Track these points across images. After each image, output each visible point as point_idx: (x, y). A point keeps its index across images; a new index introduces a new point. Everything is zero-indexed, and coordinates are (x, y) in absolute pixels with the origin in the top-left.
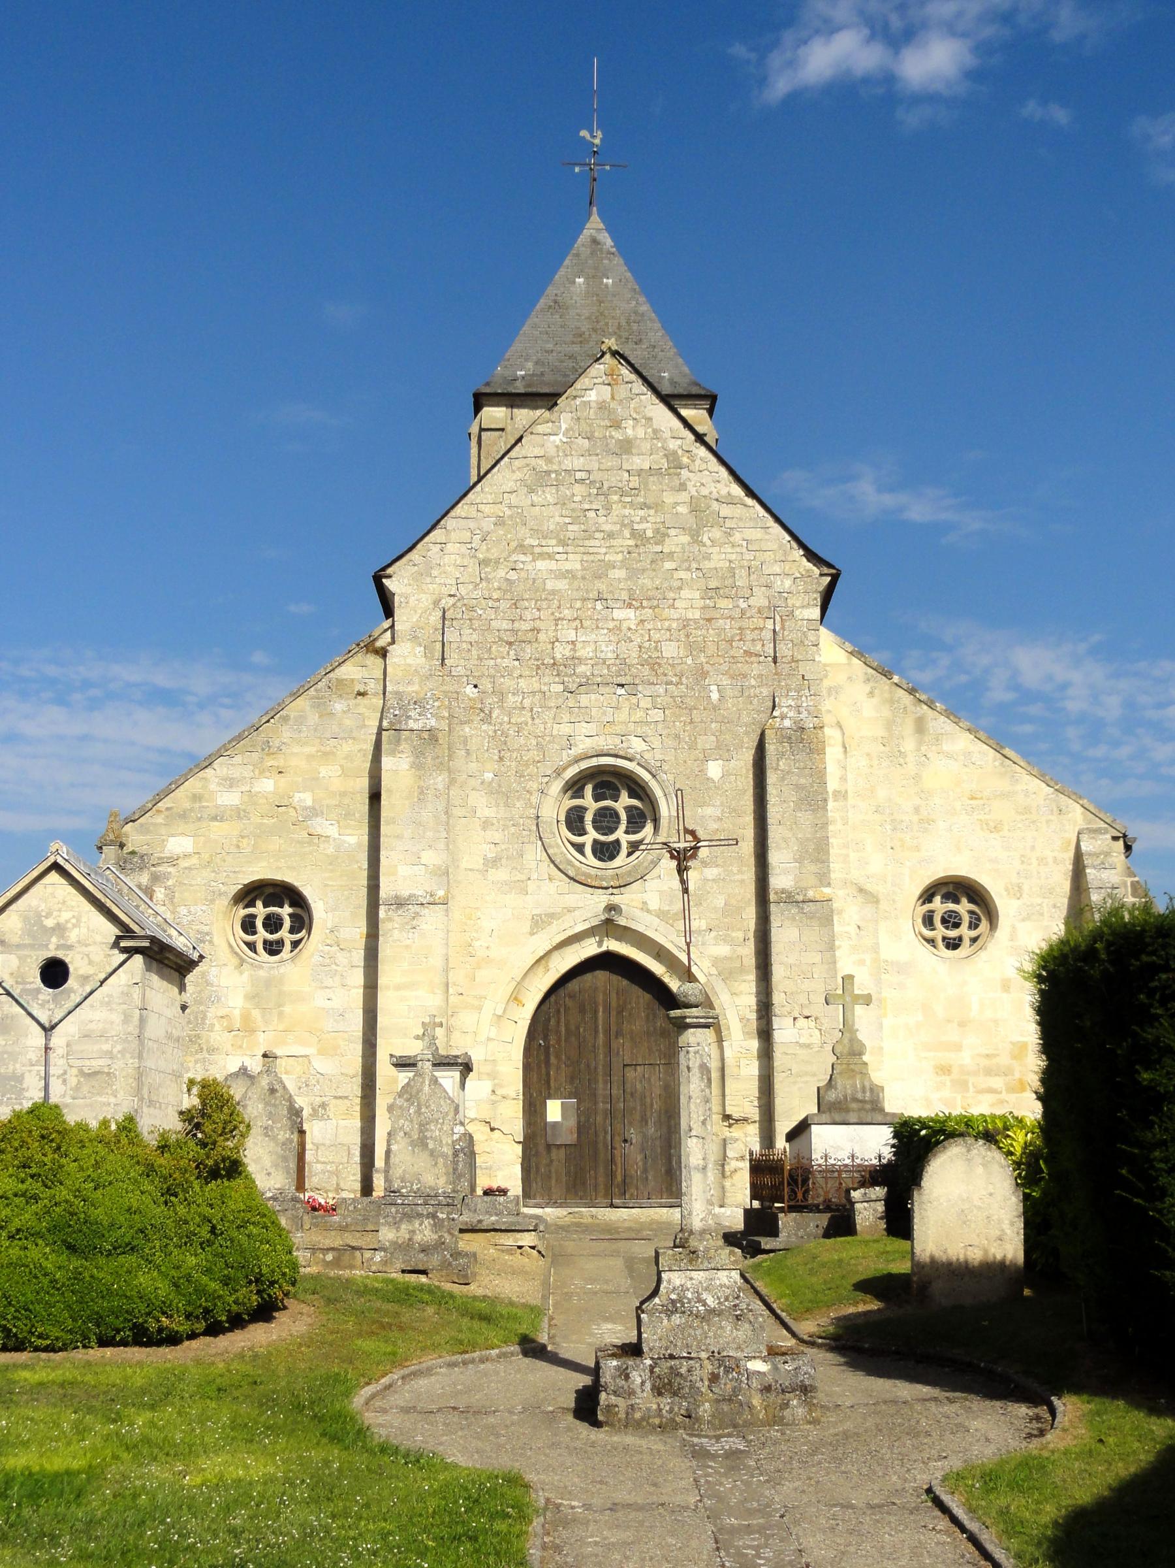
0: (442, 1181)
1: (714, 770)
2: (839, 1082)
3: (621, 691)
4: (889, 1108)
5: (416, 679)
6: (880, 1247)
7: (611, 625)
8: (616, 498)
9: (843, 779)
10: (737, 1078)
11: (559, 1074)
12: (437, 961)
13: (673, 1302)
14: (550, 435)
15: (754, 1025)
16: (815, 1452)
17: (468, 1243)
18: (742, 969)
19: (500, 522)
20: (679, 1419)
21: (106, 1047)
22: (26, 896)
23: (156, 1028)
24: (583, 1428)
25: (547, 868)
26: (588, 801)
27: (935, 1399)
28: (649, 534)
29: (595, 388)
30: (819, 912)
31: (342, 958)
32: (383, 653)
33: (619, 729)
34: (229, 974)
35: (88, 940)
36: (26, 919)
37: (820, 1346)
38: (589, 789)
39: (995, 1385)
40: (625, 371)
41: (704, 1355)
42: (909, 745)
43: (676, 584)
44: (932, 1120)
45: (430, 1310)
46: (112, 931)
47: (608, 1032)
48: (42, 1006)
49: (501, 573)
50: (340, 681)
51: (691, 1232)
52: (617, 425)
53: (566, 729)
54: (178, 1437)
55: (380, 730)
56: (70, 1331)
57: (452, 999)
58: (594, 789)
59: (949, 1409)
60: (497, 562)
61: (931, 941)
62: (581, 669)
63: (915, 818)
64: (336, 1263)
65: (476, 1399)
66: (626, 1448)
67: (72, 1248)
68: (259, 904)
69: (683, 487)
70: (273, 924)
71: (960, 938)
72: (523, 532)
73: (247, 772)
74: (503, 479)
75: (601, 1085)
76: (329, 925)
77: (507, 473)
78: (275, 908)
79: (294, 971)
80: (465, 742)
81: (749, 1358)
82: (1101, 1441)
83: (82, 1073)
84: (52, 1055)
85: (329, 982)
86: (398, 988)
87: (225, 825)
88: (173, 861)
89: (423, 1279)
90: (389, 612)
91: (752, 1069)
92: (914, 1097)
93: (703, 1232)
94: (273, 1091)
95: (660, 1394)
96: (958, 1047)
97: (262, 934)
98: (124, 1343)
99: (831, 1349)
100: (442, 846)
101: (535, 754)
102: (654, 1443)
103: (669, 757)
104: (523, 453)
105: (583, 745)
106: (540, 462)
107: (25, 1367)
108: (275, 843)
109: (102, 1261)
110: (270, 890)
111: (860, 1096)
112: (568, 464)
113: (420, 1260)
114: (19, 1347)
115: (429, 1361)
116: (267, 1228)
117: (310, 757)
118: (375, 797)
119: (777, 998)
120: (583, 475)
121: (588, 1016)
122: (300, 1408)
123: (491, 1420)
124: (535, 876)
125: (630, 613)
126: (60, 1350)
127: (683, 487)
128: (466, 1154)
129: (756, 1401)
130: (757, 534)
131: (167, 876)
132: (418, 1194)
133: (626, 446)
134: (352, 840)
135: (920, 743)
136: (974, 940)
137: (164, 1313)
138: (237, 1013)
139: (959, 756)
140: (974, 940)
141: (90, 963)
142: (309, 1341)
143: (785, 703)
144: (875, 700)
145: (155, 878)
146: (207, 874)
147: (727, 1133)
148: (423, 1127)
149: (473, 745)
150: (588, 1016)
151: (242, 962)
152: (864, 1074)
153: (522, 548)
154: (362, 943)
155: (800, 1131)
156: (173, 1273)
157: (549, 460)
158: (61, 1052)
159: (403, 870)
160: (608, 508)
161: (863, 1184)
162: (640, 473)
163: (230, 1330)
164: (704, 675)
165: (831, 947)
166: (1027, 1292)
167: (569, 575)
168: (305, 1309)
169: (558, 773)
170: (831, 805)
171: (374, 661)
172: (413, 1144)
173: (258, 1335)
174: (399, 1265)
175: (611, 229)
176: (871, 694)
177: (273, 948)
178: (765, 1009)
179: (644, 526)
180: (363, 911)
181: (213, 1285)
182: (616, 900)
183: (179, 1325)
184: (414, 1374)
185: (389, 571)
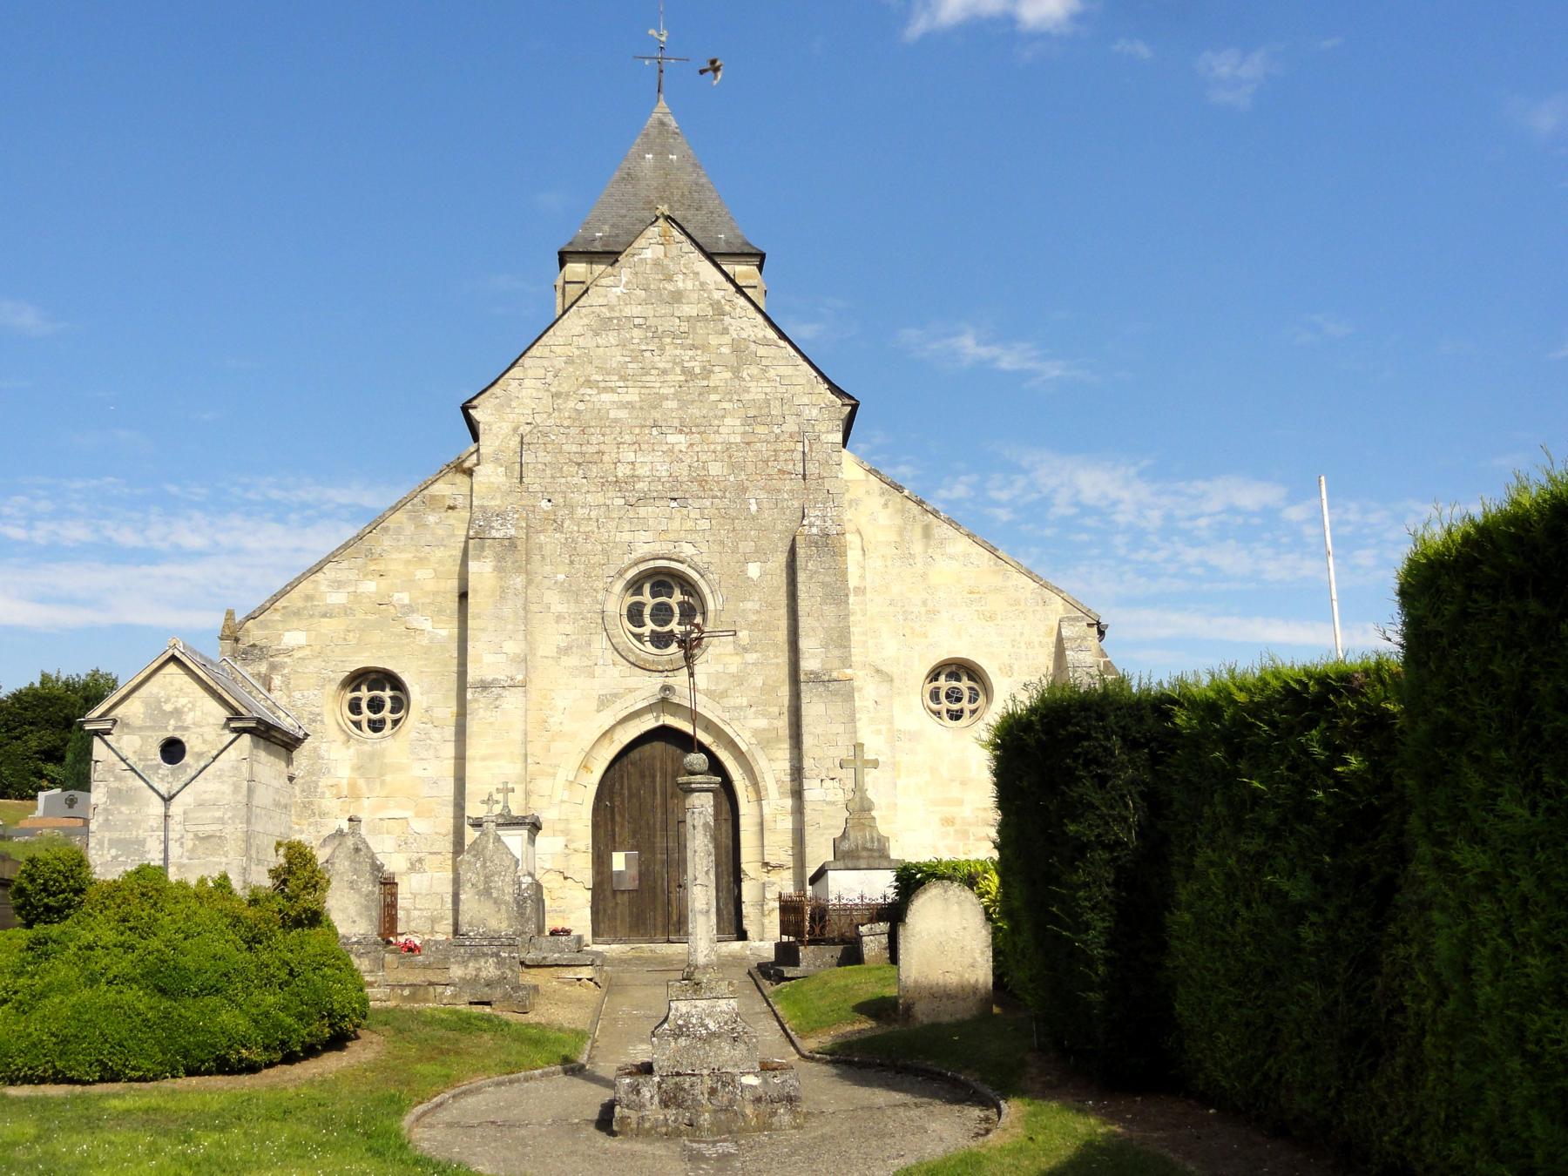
0: (504, 925)
1: (753, 570)
2: (852, 834)
3: (673, 504)
4: (895, 854)
5: (498, 495)
6: (880, 973)
7: (665, 448)
8: (668, 340)
9: (862, 577)
10: (774, 831)
11: (623, 831)
12: (518, 737)
13: (680, 1027)
14: (612, 288)
15: (788, 786)
16: (793, 1153)
17: (529, 978)
18: (778, 739)
19: (570, 360)
20: (683, 1127)
21: (218, 814)
22: (148, 685)
23: (263, 797)
24: (602, 1139)
25: (611, 655)
26: (647, 598)
27: (905, 1105)
28: (697, 370)
29: (650, 248)
30: (841, 690)
31: (435, 734)
32: (469, 473)
33: (672, 536)
34: (335, 748)
35: (202, 722)
36: (147, 704)
37: (818, 1061)
38: (647, 588)
39: (959, 1094)
40: (676, 233)
41: (705, 1072)
42: (918, 548)
43: (720, 413)
44: (926, 865)
45: (487, 1037)
46: (224, 713)
47: (664, 793)
48: (162, 779)
49: (571, 404)
50: (433, 497)
51: (696, 967)
52: (669, 279)
53: (627, 537)
54: (237, 1154)
55: (468, 538)
56: (161, 1064)
57: (530, 768)
58: (652, 587)
59: (914, 1113)
60: (568, 395)
61: (938, 713)
62: (639, 486)
63: (923, 610)
64: (412, 997)
65: (514, 1113)
66: (633, 1155)
67: (163, 991)
68: (364, 688)
69: (725, 331)
70: (376, 705)
71: (962, 711)
72: (589, 369)
73: (352, 575)
74: (572, 324)
75: (658, 839)
76: (425, 705)
77: (575, 319)
78: (376, 692)
79: (393, 745)
80: (541, 548)
81: (743, 1074)
82: (1031, 1139)
83: (196, 836)
84: (171, 822)
85: (424, 754)
86: (484, 759)
87: (334, 621)
88: (288, 652)
89: (488, 1009)
90: (476, 438)
91: (787, 823)
92: (914, 843)
93: (706, 966)
94: (357, 850)
95: (667, 1106)
96: (960, 803)
97: (367, 714)
98: (209, 1073)
99: (834, 1063)
100: (520, 636)
101: (600, 558)
102: (659, 1149)
103: (715, 560)
104: (589, 302)
105: (642, 550)
106: (604, 310)
107: (117, 1096)
108: (377, 636)
109: (189, 1001)
110: (374, 676)
111: (869, 845)
112: (627, 311)
113: (485, 993)
114: (115, 1078)
115: (480, 1081)
116: (340, 969)
117: (408, 562)
118: (463, 596)
119: (807, 763)
120: (640, 321)
121: (647, 781)
122: (352, 1126)
123: (523, 1132)
124: (601, 662)
125: (681, 438)
126: (152, 1080)
127: (725, 331)
128: (533, 900)
129: (749, 1111)
130: (789, 371)
131: (283, 666)
132: (483, 936)
133: (677, 297)
134: (444, 633)
135: (927, 546)
136: (973, 712)
137: (244, 1046)
138: (345, 782)
139: (958, 560)
140: (973, 712)
141: (204, 741)
142: (374, 1067)
143: (813, 513)
144: (889, 510)
145: (273, 667)
146: (318, 663)
147: (765, 878)
148: (488, 879)
149: (547, 551)
150: (647, 781)
151: (349, 738)
152: (873, 827)
153: (588, 382)
154: (452, 721)
155: (821, 874)
156: (253, 1010)
157: (612, 309)
158: (178, 819)
159: (488, 658)
160: (662, 349)
161: (871, 920)
162: (689, 319)
163: (306, 1058)
164: (745, 490)
165: (853, 719)
166: (996, 1010)
167: (629, 405)
168: (375, 1038)
169: (621, 574)
170: (852, 599)
171: (461, 479)
172: (479, 893)
173: (331, 1063)
174: (467, 998)
175: (674, 112)
176: (886, 505)
177: (376, 726)
178: (797, 772)
179: (692, 364)
180: (454, 694)
181: (289, 1020)
182: (670, 681)
183: (257, 1055)
184: (464, 1093)
185: (475, 403)
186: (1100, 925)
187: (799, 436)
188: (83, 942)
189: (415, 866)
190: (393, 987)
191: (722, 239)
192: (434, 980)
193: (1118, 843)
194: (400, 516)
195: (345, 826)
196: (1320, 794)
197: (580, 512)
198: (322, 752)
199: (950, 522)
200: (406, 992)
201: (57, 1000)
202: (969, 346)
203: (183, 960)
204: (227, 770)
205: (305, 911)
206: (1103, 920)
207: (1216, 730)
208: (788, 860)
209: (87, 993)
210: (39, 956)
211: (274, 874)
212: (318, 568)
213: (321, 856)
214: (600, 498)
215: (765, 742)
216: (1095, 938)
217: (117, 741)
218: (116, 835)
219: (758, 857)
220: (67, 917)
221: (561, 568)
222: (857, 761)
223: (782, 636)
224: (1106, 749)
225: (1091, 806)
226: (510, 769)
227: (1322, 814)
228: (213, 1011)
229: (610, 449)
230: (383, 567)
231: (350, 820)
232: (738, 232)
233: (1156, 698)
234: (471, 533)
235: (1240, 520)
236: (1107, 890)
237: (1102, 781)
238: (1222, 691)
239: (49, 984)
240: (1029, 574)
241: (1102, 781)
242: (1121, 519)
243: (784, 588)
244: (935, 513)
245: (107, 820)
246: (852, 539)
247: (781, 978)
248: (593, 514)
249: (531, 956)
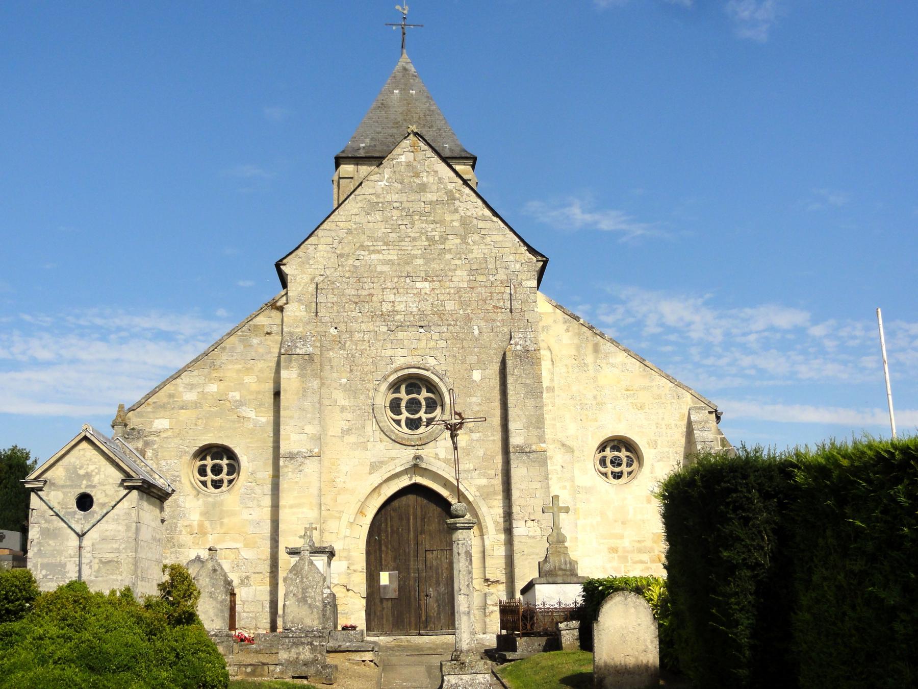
0: (316, 623)
1: (476, 375)
2: (551, 559)
3: (421, 330)
5: (301, 325)
6: (576, 657)
7: (415, 291)
8: (417, 217)
9: (552, 380)
10: (492, 557)
11: (387, 557)
14: (378, 182)
15: (502, 526)
17: (331, 659)
18: (495, 493)
19: (349, 232)
21: (116, 546)
23: (145, 534)
25: (379, 435)
26: (403, 395)
28: (437, 238)
30: (539, 459)
31: (258, 490)
32: (281, 309)
33: (420, 352)
34: (190, 501)
35: (105, 481)
40: (422, 144)
42: (590, 359)
43: (453, 267)
44: (605, 580)
47: (416, 531)
48: (77, 522)
49: (350, 262)
50: (256, 326)
51: (461, 652)
52: (417, 175)
53: (389, 353)
55: (280, 354)
57: (324, 513)
58: (406, 388)
60: (348, 255)
61: (605, 474)
62: (398, 317)
63: (594, 403)
64: (253, 674)
67: (92, 669)
68: (209, 458)
69: (456, 211)
70: (217, 470)
71: (622, 472)
74: (351, 206)
76: (250, 470)
78: (218, 461)
79: (229, 498)
80: (330, 361)
83: (101, 561)
84: (83, 551)
85: (250, 504)
86: (291, 507)
87: (188, 412)
88: (157, 433)
89: (305, 682)
90: (285, 285)
91: (501, 551)
92: (595, 567)
93: (468, 651)
94: (215, 570)
96: (622, 537)
97: (210, 476)
100: (316, 422)
101: (371, 368)
103: (450, 368)
104: (363, 192)
105: (400, 362)
106: (372, 197)
108: (218, 422)
109: (110, 676)
110: (215, 450)
111: (563, 567)
113: (303, 670)
116: (210, 654)
117: (238, 371)
118: (277, 394)
119: (515, 509)
125: (426, 284)
127: (456, 211)
128: (331, 605)
130: (499, 238)
131: (153, 443)
133: (423, 188)
134: (264, 420)
135: (596, 358)
136: (630, 473)
138: (195, 523)
139: (618, 368)
140: (630, 473)
141: (106, 495)
143: (517, 336)
144: (570, 334)
145: (147, 444)
147: (486, 590)
148: (304, 590)
149: (335, 363)
151: (199, 493)
152: (566, 554)
153: (362, 247)
155: (529, 588)
156: (153, 682)
157: (378, 196)
159: (294, 437)
160: (413, 223)
162: (431, 203)
164: (470, 320)
165: (546, 479)
166: (661, 682)
167: (390, 262)
169: (385, 378)
170: (545, 395)
171: (275, 314)
172: (299, 601)
174: (291, 674)
176: (567, 330)
177: (217, 485)
178: (508, 516)
179: (434, 234)
180: (271, 462)
182: (420, 452)
185: (284, 261)
186: (746, 622)
187: (508, 283)
188: (36, 634)
189: (245, 581)
190: (240, 666)
191: (447, 147)
192: (265, 661)
193: (758, 564)
194: (233, 339)
195: (204, 554)
196: (906, 530)
197: (357, 336)
198: (180, 503)
199: (612, 341)
200: (249, 670)
201: (19, 675)
202: (578, 215)
203: (107, 647)
204: (123, 513)
205: (184, 613)
206: (748, 618)
207: (826, 485)
208: (501, 575)
209: (40, 670)
210: (7, 644)
211: (162, 587)
212: (178, 375)
213: (192, 572)
214: (371, 326)
215: (486, 495)
216: (742, 633)
217: (47, 495)
218: (46, 561)
219: (482, 576)
220: (21, 617)
221: (344, 374)
222: (554, 507)
223: (497, 421)
224: (748, 499)
225: (738, 539)
226: (311, 514)
227: (909, 545)
228: (126, 682)
229: (377, 292)
230: (222, 375)
231: (210, 549)
232: (459, 142)
233: (781, 463)
234: (283, 351)
235: (778, 336)
236: (750, 598)
237: (746, 521)
238: (829, 458)
239: (14, 663)
240: (667, 377)
241: (746, 521)
242: (694, 335)
243: (498, 388)
244: (602, 335)
245: (40, 550)
246: (544, 353)
247: (504, 660)
248: (366, 337)
249: (330, 644)
